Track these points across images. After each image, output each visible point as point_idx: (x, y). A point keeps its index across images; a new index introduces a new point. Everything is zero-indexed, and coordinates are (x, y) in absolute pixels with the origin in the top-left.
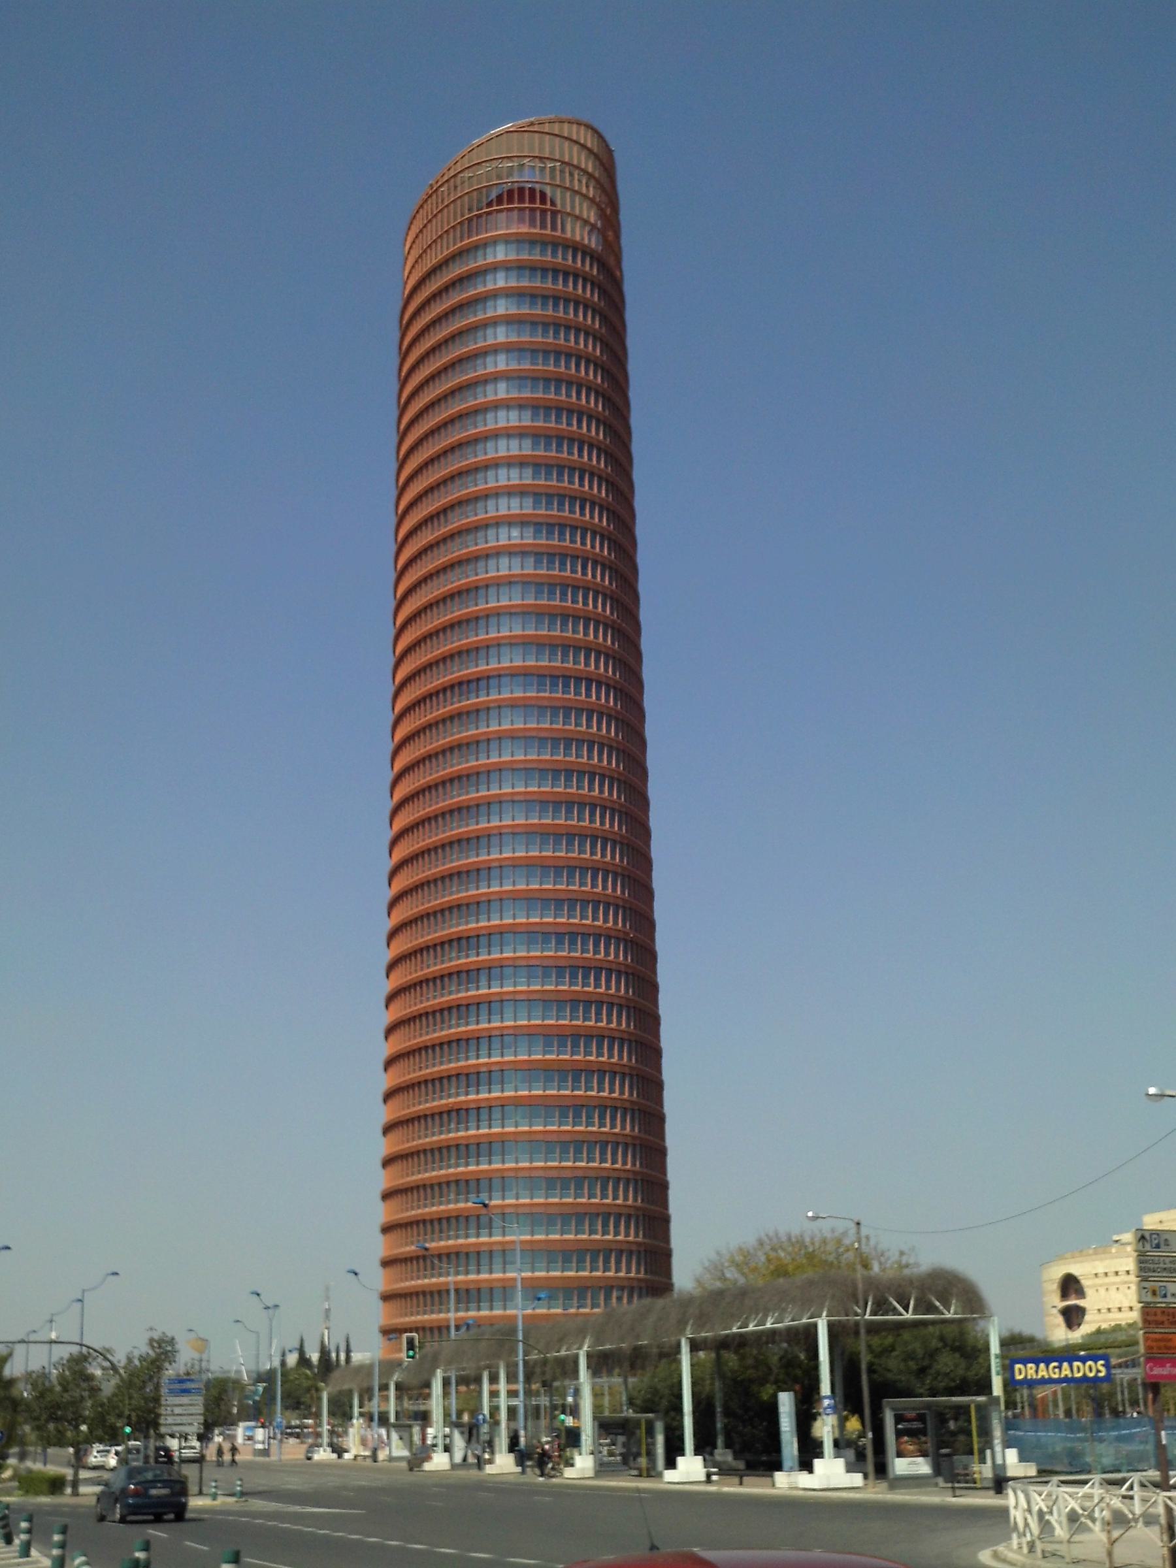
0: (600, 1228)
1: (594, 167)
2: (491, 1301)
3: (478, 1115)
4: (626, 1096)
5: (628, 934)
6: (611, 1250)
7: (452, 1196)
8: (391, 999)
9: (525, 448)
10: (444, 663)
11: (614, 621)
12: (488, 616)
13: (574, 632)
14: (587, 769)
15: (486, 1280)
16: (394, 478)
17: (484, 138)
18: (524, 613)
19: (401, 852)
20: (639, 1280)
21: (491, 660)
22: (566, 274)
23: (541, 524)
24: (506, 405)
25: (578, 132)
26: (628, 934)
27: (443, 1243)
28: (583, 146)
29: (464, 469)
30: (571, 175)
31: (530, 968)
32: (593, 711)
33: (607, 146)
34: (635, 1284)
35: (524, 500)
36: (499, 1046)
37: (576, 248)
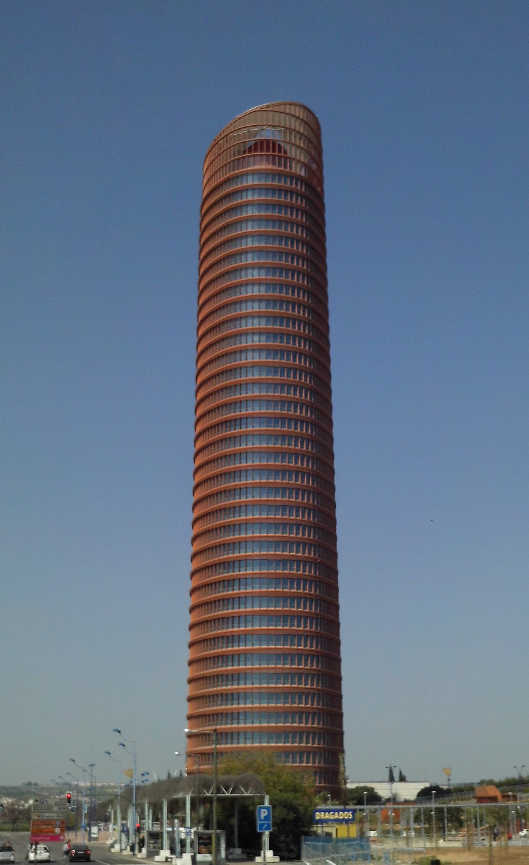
0: (297, 720)
1: (304, 129)
2: (239, 700)
3: (234, 564)
4: (313, 592)
5: (317, 560)
6: (304, 732)
7: (221, 589)
8: (194, 556)
9: (262, 308)
10: (218, 444)
11: (311, 387)
12: (240, 436)
13: (288, 410)
14: (294, 434)
15: (236, 689)
16: (198, 255)
17: (242, 115)
18: (260, 235)
19: (200, 477)
20: (319, 728)
21: (242, 443)
22: (286, 192)
23: (269, 284)
24: (253, 267)
25: (295, 110)
26: (317, 560)
27: (215, 651)
28: (298, 118)
29: (229, 335)
30: (290, 134)
31: (260, 578)
32: (297, 403)
33: (313, 115)
34: (317, 711)
35: (261, 337)
36: (245, 475)
37: (293, 177)
